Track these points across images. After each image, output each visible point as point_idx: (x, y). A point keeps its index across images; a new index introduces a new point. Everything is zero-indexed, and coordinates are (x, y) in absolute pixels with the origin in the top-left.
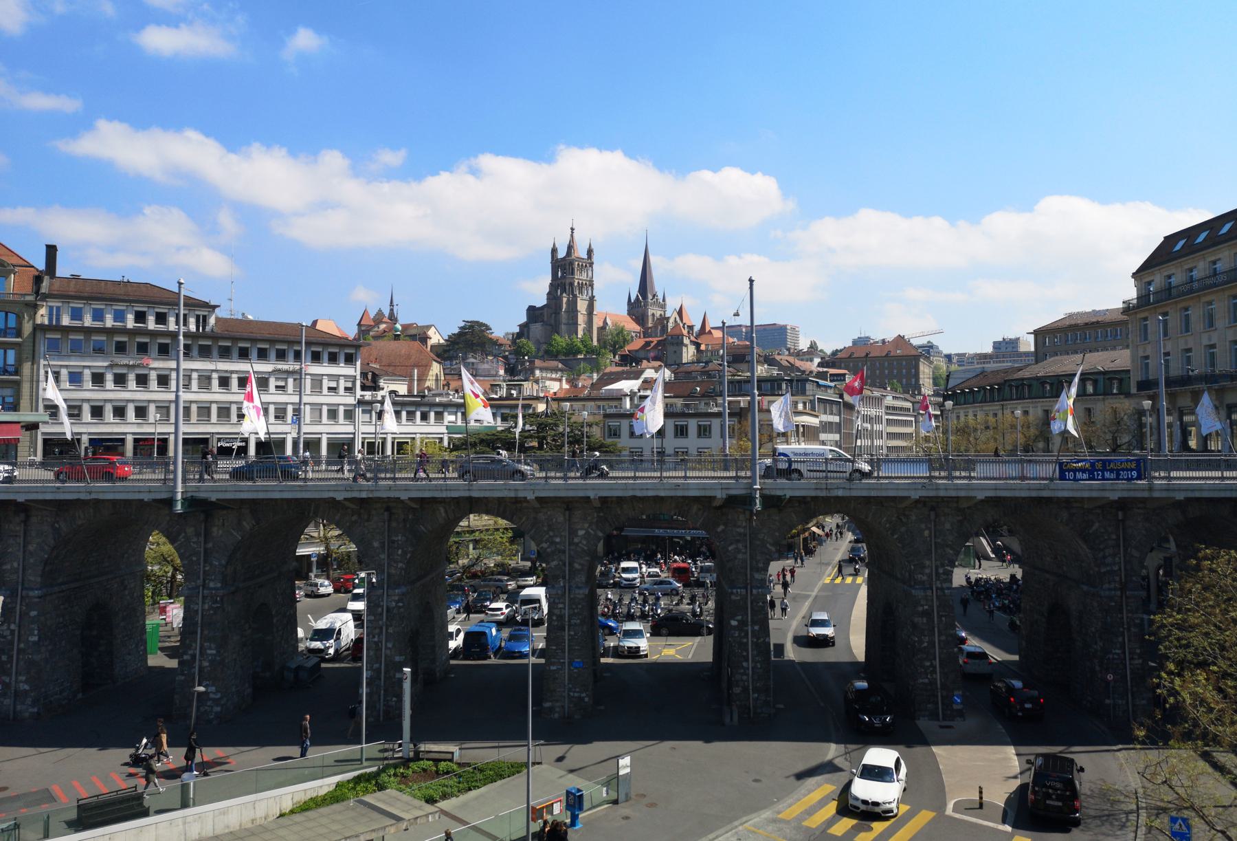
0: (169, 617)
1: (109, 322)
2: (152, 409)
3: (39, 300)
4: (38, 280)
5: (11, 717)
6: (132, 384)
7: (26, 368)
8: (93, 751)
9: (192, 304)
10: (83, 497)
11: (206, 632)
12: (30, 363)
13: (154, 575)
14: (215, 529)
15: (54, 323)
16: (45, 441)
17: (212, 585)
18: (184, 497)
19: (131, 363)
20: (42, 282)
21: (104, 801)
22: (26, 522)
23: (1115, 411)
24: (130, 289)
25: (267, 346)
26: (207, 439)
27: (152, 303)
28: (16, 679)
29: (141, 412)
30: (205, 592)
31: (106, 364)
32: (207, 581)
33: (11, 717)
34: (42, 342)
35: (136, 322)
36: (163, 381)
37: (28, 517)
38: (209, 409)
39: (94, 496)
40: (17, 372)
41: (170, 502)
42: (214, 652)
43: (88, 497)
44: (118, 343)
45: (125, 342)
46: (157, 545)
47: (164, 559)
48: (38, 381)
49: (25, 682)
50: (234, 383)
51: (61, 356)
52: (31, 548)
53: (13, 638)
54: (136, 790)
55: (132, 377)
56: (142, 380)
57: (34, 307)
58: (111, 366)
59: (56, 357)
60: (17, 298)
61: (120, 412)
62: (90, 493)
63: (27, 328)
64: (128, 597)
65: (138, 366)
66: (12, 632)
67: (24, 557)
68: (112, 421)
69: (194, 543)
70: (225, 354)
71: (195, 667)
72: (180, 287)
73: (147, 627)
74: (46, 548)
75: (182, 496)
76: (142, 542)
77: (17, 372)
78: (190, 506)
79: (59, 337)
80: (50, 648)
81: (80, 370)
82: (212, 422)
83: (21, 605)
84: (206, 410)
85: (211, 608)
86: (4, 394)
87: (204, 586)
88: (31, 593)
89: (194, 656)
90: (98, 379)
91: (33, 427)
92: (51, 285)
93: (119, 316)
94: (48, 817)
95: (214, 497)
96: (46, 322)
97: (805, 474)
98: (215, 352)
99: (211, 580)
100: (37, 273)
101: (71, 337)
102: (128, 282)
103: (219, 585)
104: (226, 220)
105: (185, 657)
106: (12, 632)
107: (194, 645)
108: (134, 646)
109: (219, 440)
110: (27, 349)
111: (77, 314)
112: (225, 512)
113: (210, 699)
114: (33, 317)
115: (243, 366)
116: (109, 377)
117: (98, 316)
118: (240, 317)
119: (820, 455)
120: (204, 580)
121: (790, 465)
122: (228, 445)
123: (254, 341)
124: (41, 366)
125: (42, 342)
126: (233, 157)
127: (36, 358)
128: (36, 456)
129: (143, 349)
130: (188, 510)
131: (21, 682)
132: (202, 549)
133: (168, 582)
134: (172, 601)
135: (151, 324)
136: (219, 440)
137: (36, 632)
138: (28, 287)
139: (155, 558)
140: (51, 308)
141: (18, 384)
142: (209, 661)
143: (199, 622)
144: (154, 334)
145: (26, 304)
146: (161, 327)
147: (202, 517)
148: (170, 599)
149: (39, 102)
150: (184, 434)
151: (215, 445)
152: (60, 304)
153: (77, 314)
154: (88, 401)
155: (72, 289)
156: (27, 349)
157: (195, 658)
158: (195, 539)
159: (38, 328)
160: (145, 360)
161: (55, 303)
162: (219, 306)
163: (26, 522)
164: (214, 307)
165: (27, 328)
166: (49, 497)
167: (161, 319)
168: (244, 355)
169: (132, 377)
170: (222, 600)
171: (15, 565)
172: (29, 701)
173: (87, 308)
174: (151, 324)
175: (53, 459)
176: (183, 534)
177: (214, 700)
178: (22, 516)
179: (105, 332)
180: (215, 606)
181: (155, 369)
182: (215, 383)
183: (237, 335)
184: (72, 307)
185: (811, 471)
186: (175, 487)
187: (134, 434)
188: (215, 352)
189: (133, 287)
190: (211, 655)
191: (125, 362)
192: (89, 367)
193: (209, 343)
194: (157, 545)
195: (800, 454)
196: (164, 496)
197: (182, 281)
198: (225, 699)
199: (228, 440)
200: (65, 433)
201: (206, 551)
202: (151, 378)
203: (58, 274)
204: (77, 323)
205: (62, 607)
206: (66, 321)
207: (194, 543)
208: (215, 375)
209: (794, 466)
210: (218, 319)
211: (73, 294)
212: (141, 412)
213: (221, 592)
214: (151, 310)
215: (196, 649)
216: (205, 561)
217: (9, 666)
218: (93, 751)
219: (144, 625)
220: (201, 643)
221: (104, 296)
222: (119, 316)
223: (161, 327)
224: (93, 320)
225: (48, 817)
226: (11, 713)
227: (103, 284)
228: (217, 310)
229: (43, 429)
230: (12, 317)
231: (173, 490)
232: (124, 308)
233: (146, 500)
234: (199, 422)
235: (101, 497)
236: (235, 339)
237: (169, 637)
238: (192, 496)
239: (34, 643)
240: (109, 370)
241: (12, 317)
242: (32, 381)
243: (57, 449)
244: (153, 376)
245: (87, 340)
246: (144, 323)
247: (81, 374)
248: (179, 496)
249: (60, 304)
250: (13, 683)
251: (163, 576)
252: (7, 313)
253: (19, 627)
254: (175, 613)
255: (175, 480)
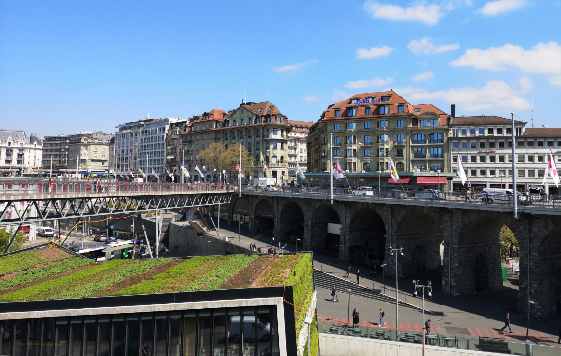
0: (511, 265)
1: (477, 134)
2: (497, 171)
3: (450, 127)
4: (449, 119)
5: (449, 295)
6: (488, 160)
7: (446, 155)
8: (483, 318)
9: (517, 123)
10: (474, 208)
11: (532, 276)
12: (447, 153)
13: (502, 246)
14: (534, 228)
15: (455, 136)
16: (454, 184)
17: (533, 254)
18: (519, 211)
19: (487, 151)
20: (450, 120)
21: (491, 341)
22: (451, 217)
23: (546, 168)
24: (486, 119)
25: (494, 141)
26: (524, 185)
27: (495, 124)
28: (451, 280)
29: (493, 173)
30: (530, 257)
31: (477, 152)
32: (531, 252)
33: (449, 295)
34: (451, 144)
35: (489, 133)
36: (502, 159)
37: (452, 215)
38: (524, 171)
39: (478, 208)
40: (442, 157)
41: (512, 213)
42: (536, 286)
43: (476, 209)
44: (481, 143)
45: (485, 142)
46: (506, 232)
47: (507, 239)
48: (450, 160)
49: (454, 282)
50: (536, 159)
51: (467, 149)
52: (454, 228)
53: (449, 263)
54: (504, 341)
55: (488, 157)
56: (492, 159)
57: (448, 130)
58: (479, 153)
59: (465, 150)
60: (441, 127)
61: (483, 172)
62: (477, 207)
63: (445, 139)
64: (493, 254)
65: (490, 152)
66: (448, 260)
67: (451, 232)
68: (480, 176)
69: (524, 233)
70: (531, 145)
71: (527, 291)
72: (512, 116)
73: (502, 268)
74: (459, 228)
75: (517, 211)
76: (498, 230)
77: (442, 157)
78: (521, 216)
79: (458, 142)
80: (463, 270)
81: (467, 155)
82: (526, 177)
83: (451, 250)
84: (532, 172)
85: (533, 265)
86: (438, 166)
87: (530, 254)
88: (454, 246)
89: (526, 286)
90: (474, 158)
91: (450, 178)
92: (453, 121)
93: (482, 131)
94: (468, 340)
95: (533, 213)
96: (452, 136)
97: (495, 201)
98: (526, 145)
99: (533, 252)
100: (448, 117)
101: (462, 141)
102: (484, 116)
103: (537, 255)
104: (525, 83)
105: (522, 286)
106: (448, 260)
107: (526, 281)
108: (497, 276)
109: (530, 186)
110: (446, 148)
111: (464, 132)
112: (538, 220)
113: (536, 308)
114: (447, 135)
115: (531, 151)
116: (478, 158)
117: (473, 132)
118: (542, 127)
119: (501, 193)
120: (530, 251)
121: (487, 197)
122: (534, 188)
123: (546, 138)
124: (451, 154)
125: (451, 144)
126: (529, 52)
127: (449, 151)
128: (451, 190)
129: (492, 145)
130: (521, 218)
131: (452, 281)
132: (528, 237)
133: (508, 250)
134: (512, 258)
135: (496, 134)
136: (530, 186)
137: (457, 262)
138: (445, 123)
139: (503, 238)
140: (454, 130)
141: (442, 162)
142: (534, 290)
143: (528, 270)
144: (497, 138)
145: (445, 130)
146: (500, 135)
147: (527, 222)
148: (510, 257)
149: (444, 49)
150: (517, 183)
151: (528, 188)
152: (457, 128)
153: (464, 132)
154: (470, 168)
155: (462, 122)
156: (446, 148)
157: (527, 287)
158: (524, 232)
159: (450, 139)
160: (493, 150)
161: (455, 128)
162: (527, 123)
163: (451, 217)
164: (525, 124)
165: (445, 139)
166: (460, 207)
167: (500, 131)
168: (541, 145)
169: (488, 157)
170: (539, 262)
171: (448, 234)
172: (456, 290)
173: (468, 129)
174: (496, 134)
175: (457, 192)
176: (518, 229)
177: (538, 309)
178: (450, 215)
179: (466, 139)
180: (536, 264)
181: (498, 153)
182: (526, 159)
183: (537, 136)
184: (462, 129)
185: (497, 200)
186: (514, 207)
187: (490, 182)
188: (526, 145)
189: (486, 118)
190: (535, 287)
191: (485, 151)
192: (470, 154)
193: (533, 140)
194: (506, 232)
195: (493, 192)
196: (509, 210)
197: (513, 113)
198: (543, 310)
199: (534, 186)
200: (461, 182)
201: (530, 238)
202: (496, 158)
203: (456, 116)
204: (464, 136)
205: (466, 254)
206: (460, 135)
207: (524, 233)
208: (526, 156)
209: (489, 197)
210: (526, 129)
211: (462, 123)
212: (493, 173)
213: (539, 258)
214: (495, 128)
215: (527, 283)
216: (530, 243)
217: (447, 274)
218: (483, 318)
219: (501, 267)
220: (529, 281)
221: (475, 123)
222: (482, 131)
223: (500, 135)
224: (471, 134)
225: (468, 340)
226: (449, 293)
227: (474, 118)
228: (526, 125)
229: (454, 179)
230: (440, 135)
231: (513, 208)
232: (484, 128)
233: (501, 212)
234: (500, 177)
235: (481, 209)
236: (535, 138)
237: (511, 275)
238: (522, 212)
239: (457, 267)
240: (478, 155)
241: (440, 135)
242: (448, 160)
243: (459, 188)
244: (497, 157)
245: (469, 142)
246: (492, 133)
247: (466, 157)
248: (516, 211)
249: (457, 128)
250: (450, 281)
251: (506, 247)
252: (438, 134)
253: (451, 259)
254: (515, 265)
255: (514, 204)
